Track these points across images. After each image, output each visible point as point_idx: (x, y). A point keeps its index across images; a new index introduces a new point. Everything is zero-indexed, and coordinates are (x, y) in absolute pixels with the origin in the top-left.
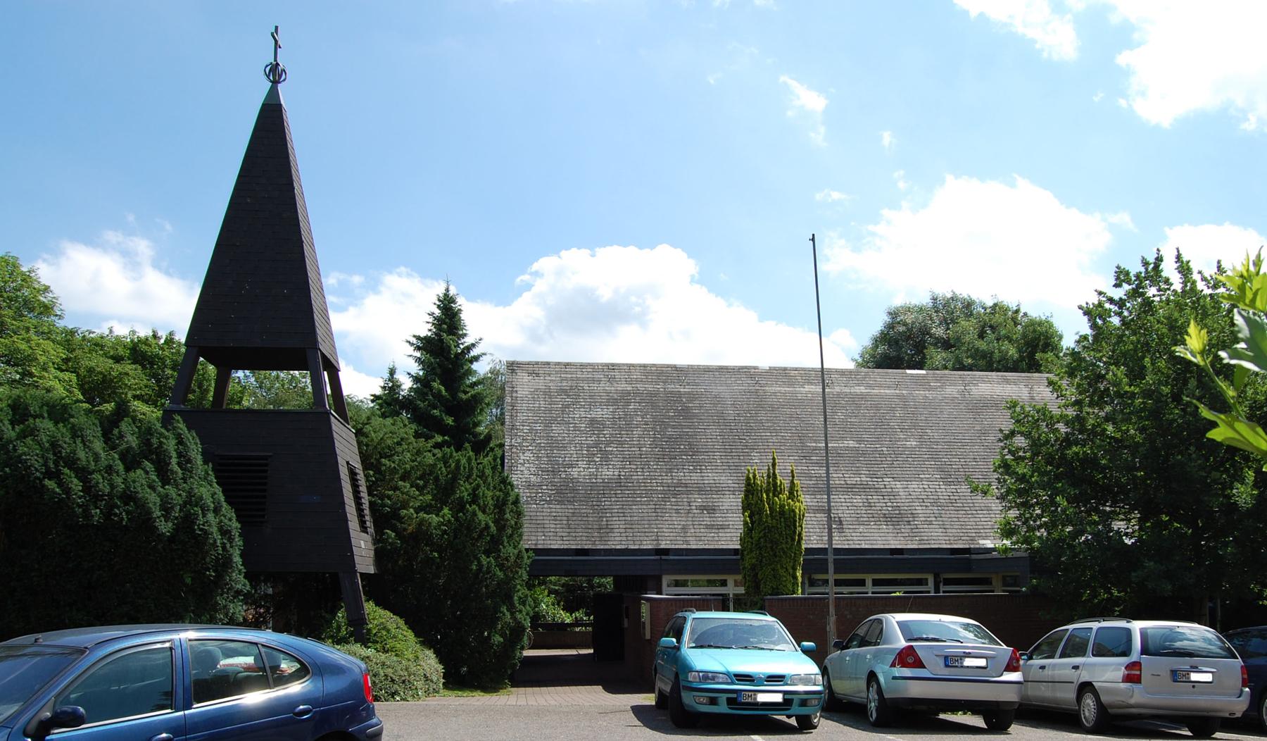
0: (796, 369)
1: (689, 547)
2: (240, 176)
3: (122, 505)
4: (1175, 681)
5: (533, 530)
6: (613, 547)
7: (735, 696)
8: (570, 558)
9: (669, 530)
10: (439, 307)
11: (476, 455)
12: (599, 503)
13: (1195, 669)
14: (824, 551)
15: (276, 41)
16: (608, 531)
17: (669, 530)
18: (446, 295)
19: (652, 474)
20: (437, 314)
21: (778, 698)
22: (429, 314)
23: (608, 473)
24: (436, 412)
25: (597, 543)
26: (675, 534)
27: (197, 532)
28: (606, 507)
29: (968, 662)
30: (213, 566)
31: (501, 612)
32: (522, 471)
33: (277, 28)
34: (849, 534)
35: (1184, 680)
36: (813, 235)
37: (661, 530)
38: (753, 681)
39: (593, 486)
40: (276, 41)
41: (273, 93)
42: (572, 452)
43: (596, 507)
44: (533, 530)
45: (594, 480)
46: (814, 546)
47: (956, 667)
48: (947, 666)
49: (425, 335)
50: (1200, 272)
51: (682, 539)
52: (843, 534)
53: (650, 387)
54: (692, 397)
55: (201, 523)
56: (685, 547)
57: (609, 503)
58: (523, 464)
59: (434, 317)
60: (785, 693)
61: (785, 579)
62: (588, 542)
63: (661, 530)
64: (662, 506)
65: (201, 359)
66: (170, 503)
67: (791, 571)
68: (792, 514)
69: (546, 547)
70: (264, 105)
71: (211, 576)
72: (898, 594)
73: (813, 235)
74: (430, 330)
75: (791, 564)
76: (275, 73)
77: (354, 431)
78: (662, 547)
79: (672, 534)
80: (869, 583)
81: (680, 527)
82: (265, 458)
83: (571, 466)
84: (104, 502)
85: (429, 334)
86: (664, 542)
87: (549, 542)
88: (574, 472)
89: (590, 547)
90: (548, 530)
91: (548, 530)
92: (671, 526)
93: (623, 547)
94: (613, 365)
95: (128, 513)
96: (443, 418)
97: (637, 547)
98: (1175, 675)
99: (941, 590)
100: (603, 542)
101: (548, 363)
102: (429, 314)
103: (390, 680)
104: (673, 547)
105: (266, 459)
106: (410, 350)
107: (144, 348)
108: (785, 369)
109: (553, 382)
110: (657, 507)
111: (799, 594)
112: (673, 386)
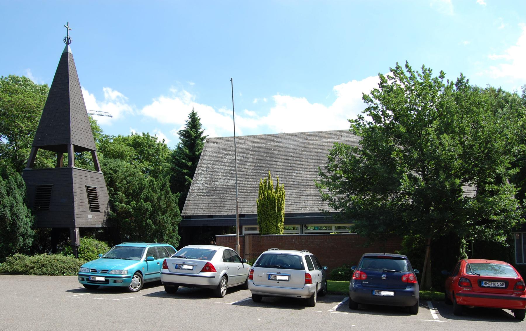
0: (326, 132)
1: (253, 213)
2: (53, 81)
4: (269, 279)
5: (194, 208)
6: (223, 214)
7: (88, 277)
8: (204, 219)
9: (247, 207)
11: (156, 179)
12: (223, 196)
13: (279, 274)
14: (234, 216)
16: (223, 207)
17: (247, 207)
18: (193, 112)
19: (248, 182)
21: (103, 279)
23: (231, 183)
25: (217, 212)
26: (249, 208)
28: (225, 197)
29: (185, 267)
32: (198, 184)
34: (325, 206)
35: (274, 279)
36: (232, 78)
37: (244, 207)
38: (96, 272)
39: (223, 189)
41: (66, 48)
42: (219, 175)
43: (221, 198)
44: (194, 208)
45: (224, 186)
46: (307, 212)
47: (179, 269)
48: (176, 268)
50: (417, 72)
51: (251, 210)
52: (323, 206)
53: (260, 145)
54: (276, 147)
56: (252, 213)
57: (227, 196)
58: (199, 181)
60: (106, 277)
61: (271, 227)
62: (214, 212)
63: (244, 207)
64: (248, 196)
67: (275, 224)
68: (273, 199)
69: (197, 215)
70: (63, 53)
72: (333, 234)
73: (232, 78)
74: (185, 128)
75: (275, 221)
76: (68, 41)
77: (103, 173)
78: (242, 214)
79: (248, 208)
80: (333, 228)
81: (252, 205)
83: (217, 181)
85: (185, 129)
86: (243, 212)
87: (198, 213)
88: (218, 183)
89: (213, 214)
90: (200, 208)
91: (200, 208)
92: (249, 205)
93: (226, 214)
94: (248, 136)
97: (232, 214)
98: (270, 277)
99: (304, 232)
100: (220, 212)
101: (222, 138)
104: (247, 213)
107: (137, 140)
108: (322, 132)
109: (222, 145)
110: (246, 196)
111: (282, 232)
112: (270, 144)
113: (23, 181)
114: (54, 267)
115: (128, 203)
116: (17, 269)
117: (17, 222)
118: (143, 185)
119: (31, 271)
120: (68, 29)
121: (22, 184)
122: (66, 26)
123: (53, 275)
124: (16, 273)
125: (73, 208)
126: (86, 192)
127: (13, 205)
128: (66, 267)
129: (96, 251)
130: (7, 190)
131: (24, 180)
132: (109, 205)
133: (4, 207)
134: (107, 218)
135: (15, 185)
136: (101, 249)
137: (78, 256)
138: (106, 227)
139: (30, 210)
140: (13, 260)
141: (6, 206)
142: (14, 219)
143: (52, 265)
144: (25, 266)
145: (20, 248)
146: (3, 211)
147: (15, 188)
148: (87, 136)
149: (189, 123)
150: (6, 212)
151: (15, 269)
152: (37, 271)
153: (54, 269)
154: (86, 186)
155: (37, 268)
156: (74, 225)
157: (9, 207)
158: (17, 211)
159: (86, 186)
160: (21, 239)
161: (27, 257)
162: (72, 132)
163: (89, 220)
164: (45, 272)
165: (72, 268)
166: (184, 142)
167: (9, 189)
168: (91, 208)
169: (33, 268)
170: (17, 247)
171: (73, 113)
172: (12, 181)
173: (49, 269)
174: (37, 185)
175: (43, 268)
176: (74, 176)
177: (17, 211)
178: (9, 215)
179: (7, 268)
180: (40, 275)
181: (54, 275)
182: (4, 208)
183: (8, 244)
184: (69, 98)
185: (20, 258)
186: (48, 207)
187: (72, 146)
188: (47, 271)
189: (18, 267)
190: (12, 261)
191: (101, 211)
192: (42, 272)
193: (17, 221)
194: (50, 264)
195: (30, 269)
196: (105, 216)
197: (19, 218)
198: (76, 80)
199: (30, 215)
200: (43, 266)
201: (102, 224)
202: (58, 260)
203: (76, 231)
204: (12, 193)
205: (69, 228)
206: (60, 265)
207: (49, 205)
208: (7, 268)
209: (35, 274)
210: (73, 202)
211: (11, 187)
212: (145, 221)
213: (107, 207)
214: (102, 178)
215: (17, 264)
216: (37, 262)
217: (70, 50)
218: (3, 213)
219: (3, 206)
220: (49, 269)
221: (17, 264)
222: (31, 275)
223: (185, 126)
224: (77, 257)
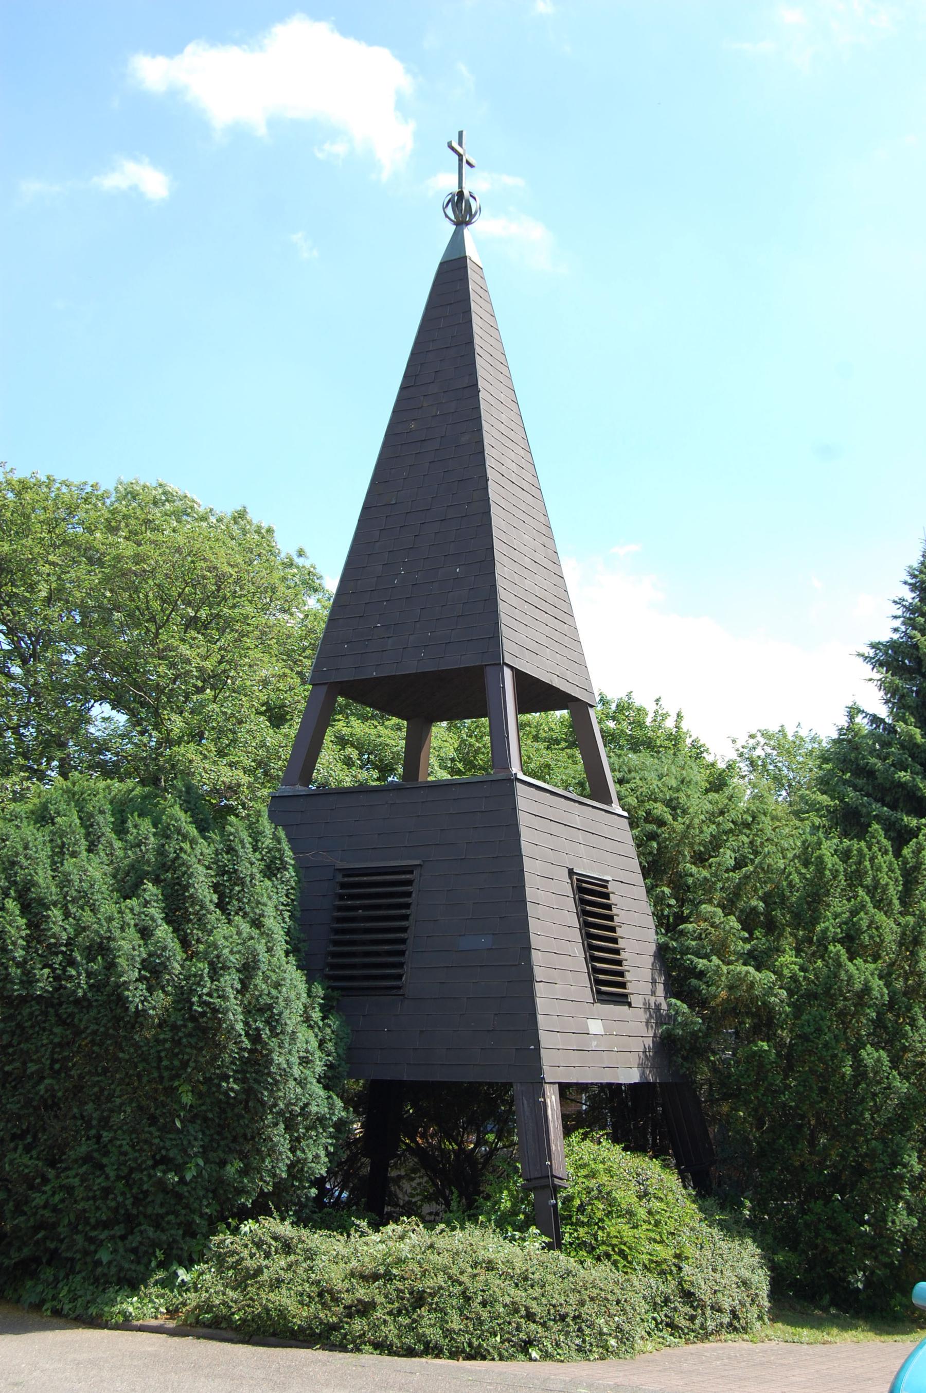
2: (403, 388)
3: (84, 961)
10: (913, 588)
15: (460, 156)
20: (910, 601)
22: (895, 602)
24: (904, 776)
27: (195, 1007)
30: (236, 1072)
31: (905, 1166)
33: (461, 134)
40: (460, 156)
41: (457, 242)
49: (888, 639)
55: (205, 991)
59: (904, 606)
65: (340, 699)
66: (159, 957)
71: (232, 1089)
74: (896, 630)
77: (626, 814)
82: (409, 870)
84: (60, 957)
85: (896, 636)
95: (89, 975)
96: (916, 786)
102: (895, 602)
103: (523, 1313)
105: (411, 872)
106: (867, 670)
113: (285, 846)
114: (476, 1305)
115: (758, 960)
116: (282, 1313)
117: (271, 1051)
118: (827, 872)
119: (358, 1325)
120: (461, 160)
121: (281, 859)
122: (455, 145)
123: (476, 1354)
124: (274, 1334)
125: (527, 980)
126: (570, 904)
127: (256, 961)
128: (535, 1308)
129: (642, 1213)
130: (216, 887)
131: (290, 840)
132: (660, 975)
133: (216, 969)
134: (655, 1036)
135: (252, 864)
136: (661, 1200)
137: (559, 1237)
138: (654, 1084)
139: (319, 990)
140: (252, 1256)
141: (225, 968)
142: (255, 1038)
143: (468, 1299)
144: (320, 1295)
145: (275, 1185)
146: (209, 995)
147: (252, 877)
148: (556, 635)
149: (910, 609)
150: (224, 997)
151: (267, 1310)
152: (390, 1332)
153: (481, 1323)
154: (571, 872)
155: (390, 1313)
156: (539, 1070)
157: (238, 971)
158: (274, 992)
159: (571, 872)
160: (279, 1137)
161: (316, 1239)
162: (502, 607)
163: (594, 1045)
164: (434, 1334)
165: (567, 1315)
166: (893, 696)
167: (230, 880)
168: (598, 982)
169: (364, 1309)
170: (261, 1179)
171: (503, 526)
172: (242, 841)
173: (456, 1323)
174: (340, 865)
175: (424, 1311)
176: (523, 819)
177: (274, 992)
178: (235, 1018)
179: (224, 1303)
180: (410, 1353)
181: (484, 1358)
182: (214, 975)
183: (223, 1163)
184: (482, 452)
185: (287, 1247)
186: (399, 977)
187: (508, 674)
188: (447, 1333)
189: (284, 1299)
190: (248, 1263)
191: (633, 999)
192: (420, 1338)
193: (273, 1043)
194: (457, 1289)
195: (350, 1316)
196: (647, 1023)
197: (282, 1032)
198: (501, 377)
199: (316, 1015)
200: (419, 1299)
201: (641, 1066)
202: (490, 1266)
203: (548, 1101)
204: (239, 900)
205: (508, 1086)
206: (507, 1300)
207: (401, 965)
208: (224, 1303)
209: (382, 1347)
210: (527, 949)
211: (236, 871)
212: (854, 1050)
213: (654, 982)
214: (626, 836)
215: (277, 1284)
216: (388, 1277)
217: (471, 251)
218: (208, 1004)
219: (212, 964)
220: (456, 1323)
221: (277, 1284)
222: (358, 1349)
223: (898, 623)
224: (556, 1244)
